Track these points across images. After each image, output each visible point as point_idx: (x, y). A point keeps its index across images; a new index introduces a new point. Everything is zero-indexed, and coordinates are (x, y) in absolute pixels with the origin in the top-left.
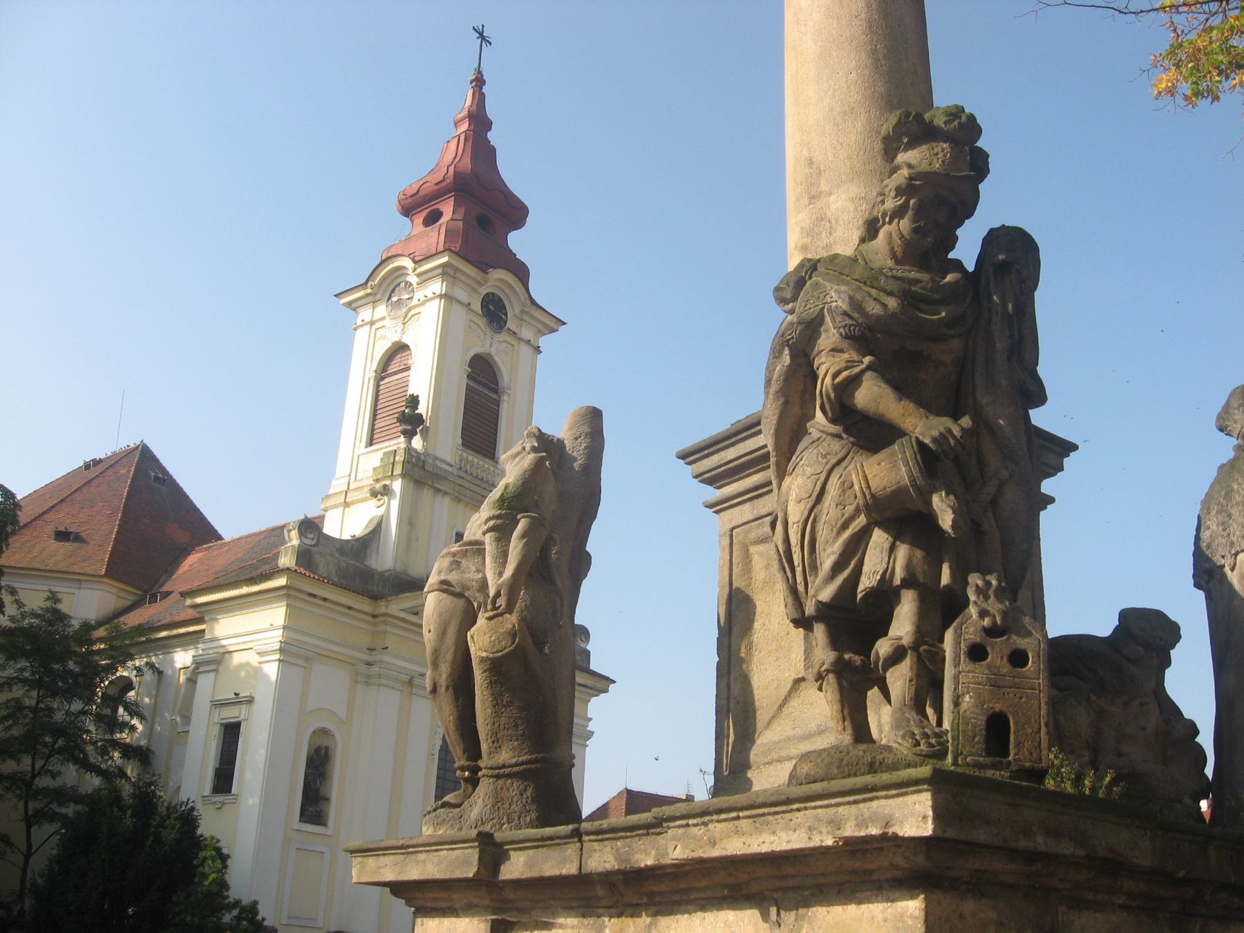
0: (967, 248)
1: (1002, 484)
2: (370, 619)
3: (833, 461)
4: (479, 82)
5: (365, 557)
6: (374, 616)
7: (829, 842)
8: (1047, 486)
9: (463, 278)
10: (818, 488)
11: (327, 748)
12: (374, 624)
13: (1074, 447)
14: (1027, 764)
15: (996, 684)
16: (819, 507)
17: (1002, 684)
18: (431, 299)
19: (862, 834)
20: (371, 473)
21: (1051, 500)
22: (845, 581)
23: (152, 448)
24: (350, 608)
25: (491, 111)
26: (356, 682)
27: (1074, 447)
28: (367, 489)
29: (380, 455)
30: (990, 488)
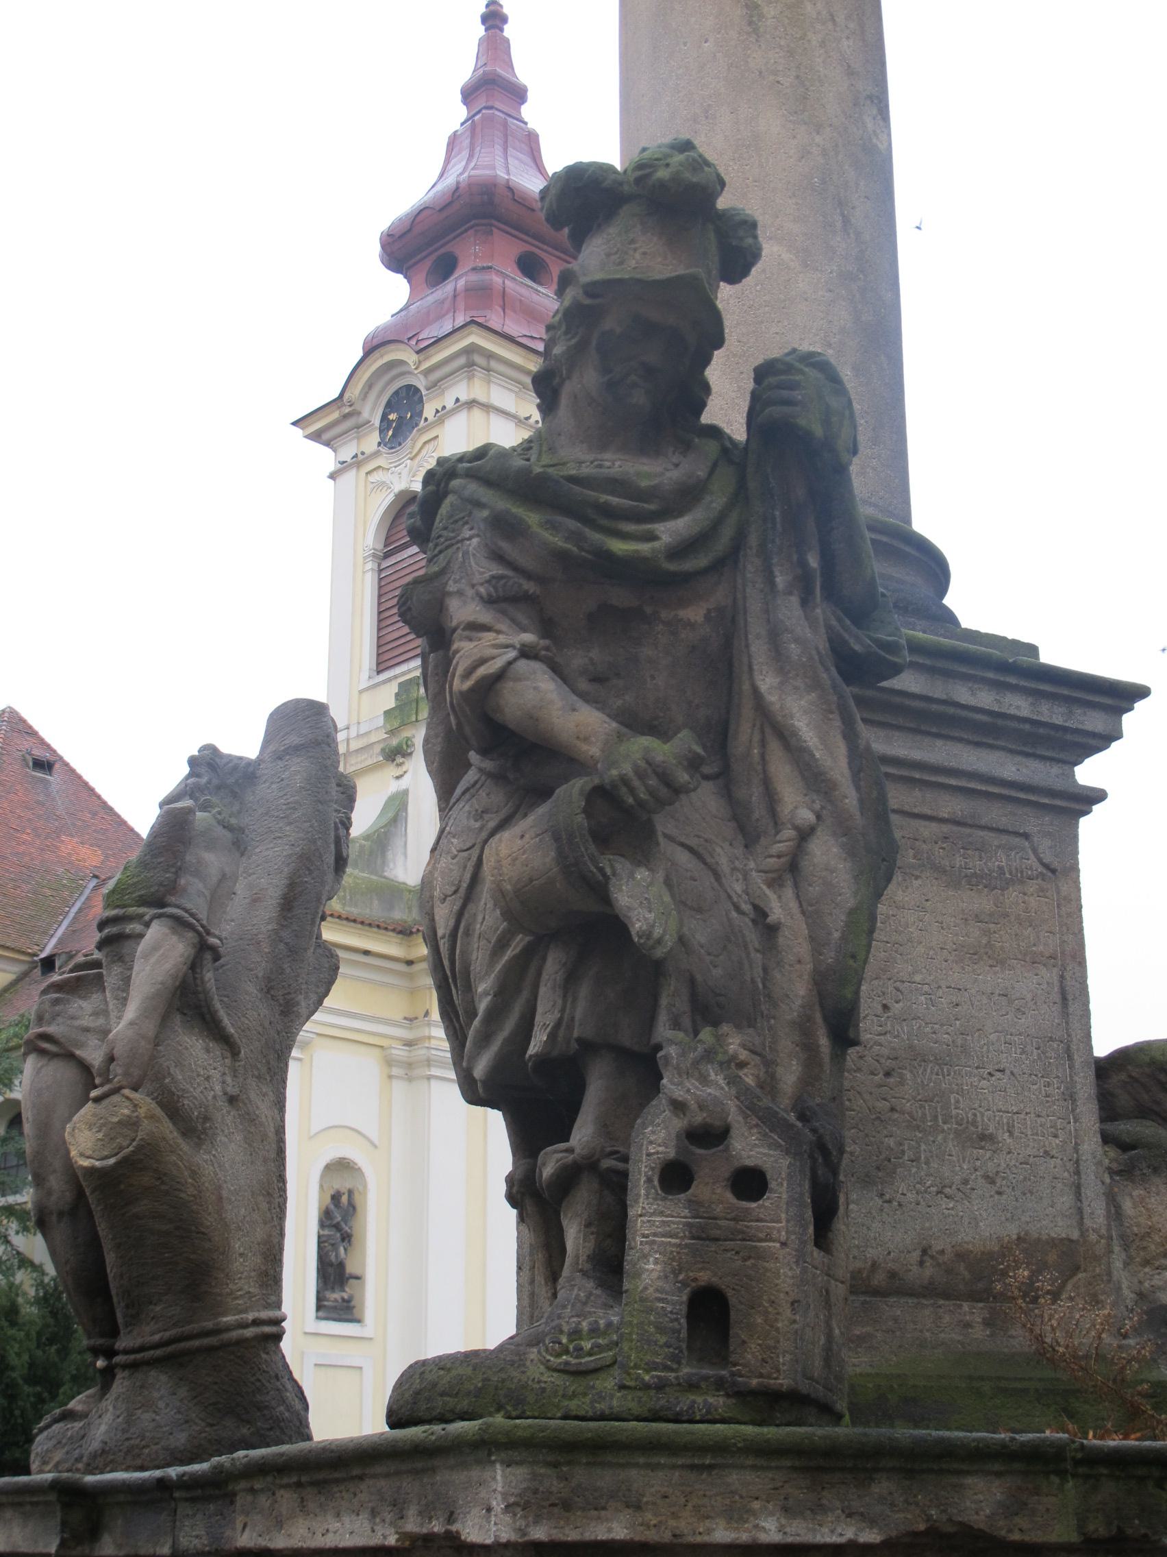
0: (727, 406)
1: (804, 835)
2: (402, 967)
3: (492, 824)
4: (494, 19)
5: (384, 863)
6: (410, 963)
7: (392, 1540)
8: (1088, 773)
9: (501, 368)
10: (468, 876)
11: (350, 1193)
12: (411, 977)
13: (1141, 692)
14: (754, 1382)
15: (703, 1234)
16: (471, 907)
17: (716, 1233)
18: (454, 411)
19: (425, 1531)
20: (381, 721)
21: (1098, 796)
22: (507, 1041)
23: (25, 714)
24: (367, 953)
25: (525, 66)
26: (390, 1077)
27: (1141, 692)
28: (377, 749)
29: (394, 688)
30: (784, 841)
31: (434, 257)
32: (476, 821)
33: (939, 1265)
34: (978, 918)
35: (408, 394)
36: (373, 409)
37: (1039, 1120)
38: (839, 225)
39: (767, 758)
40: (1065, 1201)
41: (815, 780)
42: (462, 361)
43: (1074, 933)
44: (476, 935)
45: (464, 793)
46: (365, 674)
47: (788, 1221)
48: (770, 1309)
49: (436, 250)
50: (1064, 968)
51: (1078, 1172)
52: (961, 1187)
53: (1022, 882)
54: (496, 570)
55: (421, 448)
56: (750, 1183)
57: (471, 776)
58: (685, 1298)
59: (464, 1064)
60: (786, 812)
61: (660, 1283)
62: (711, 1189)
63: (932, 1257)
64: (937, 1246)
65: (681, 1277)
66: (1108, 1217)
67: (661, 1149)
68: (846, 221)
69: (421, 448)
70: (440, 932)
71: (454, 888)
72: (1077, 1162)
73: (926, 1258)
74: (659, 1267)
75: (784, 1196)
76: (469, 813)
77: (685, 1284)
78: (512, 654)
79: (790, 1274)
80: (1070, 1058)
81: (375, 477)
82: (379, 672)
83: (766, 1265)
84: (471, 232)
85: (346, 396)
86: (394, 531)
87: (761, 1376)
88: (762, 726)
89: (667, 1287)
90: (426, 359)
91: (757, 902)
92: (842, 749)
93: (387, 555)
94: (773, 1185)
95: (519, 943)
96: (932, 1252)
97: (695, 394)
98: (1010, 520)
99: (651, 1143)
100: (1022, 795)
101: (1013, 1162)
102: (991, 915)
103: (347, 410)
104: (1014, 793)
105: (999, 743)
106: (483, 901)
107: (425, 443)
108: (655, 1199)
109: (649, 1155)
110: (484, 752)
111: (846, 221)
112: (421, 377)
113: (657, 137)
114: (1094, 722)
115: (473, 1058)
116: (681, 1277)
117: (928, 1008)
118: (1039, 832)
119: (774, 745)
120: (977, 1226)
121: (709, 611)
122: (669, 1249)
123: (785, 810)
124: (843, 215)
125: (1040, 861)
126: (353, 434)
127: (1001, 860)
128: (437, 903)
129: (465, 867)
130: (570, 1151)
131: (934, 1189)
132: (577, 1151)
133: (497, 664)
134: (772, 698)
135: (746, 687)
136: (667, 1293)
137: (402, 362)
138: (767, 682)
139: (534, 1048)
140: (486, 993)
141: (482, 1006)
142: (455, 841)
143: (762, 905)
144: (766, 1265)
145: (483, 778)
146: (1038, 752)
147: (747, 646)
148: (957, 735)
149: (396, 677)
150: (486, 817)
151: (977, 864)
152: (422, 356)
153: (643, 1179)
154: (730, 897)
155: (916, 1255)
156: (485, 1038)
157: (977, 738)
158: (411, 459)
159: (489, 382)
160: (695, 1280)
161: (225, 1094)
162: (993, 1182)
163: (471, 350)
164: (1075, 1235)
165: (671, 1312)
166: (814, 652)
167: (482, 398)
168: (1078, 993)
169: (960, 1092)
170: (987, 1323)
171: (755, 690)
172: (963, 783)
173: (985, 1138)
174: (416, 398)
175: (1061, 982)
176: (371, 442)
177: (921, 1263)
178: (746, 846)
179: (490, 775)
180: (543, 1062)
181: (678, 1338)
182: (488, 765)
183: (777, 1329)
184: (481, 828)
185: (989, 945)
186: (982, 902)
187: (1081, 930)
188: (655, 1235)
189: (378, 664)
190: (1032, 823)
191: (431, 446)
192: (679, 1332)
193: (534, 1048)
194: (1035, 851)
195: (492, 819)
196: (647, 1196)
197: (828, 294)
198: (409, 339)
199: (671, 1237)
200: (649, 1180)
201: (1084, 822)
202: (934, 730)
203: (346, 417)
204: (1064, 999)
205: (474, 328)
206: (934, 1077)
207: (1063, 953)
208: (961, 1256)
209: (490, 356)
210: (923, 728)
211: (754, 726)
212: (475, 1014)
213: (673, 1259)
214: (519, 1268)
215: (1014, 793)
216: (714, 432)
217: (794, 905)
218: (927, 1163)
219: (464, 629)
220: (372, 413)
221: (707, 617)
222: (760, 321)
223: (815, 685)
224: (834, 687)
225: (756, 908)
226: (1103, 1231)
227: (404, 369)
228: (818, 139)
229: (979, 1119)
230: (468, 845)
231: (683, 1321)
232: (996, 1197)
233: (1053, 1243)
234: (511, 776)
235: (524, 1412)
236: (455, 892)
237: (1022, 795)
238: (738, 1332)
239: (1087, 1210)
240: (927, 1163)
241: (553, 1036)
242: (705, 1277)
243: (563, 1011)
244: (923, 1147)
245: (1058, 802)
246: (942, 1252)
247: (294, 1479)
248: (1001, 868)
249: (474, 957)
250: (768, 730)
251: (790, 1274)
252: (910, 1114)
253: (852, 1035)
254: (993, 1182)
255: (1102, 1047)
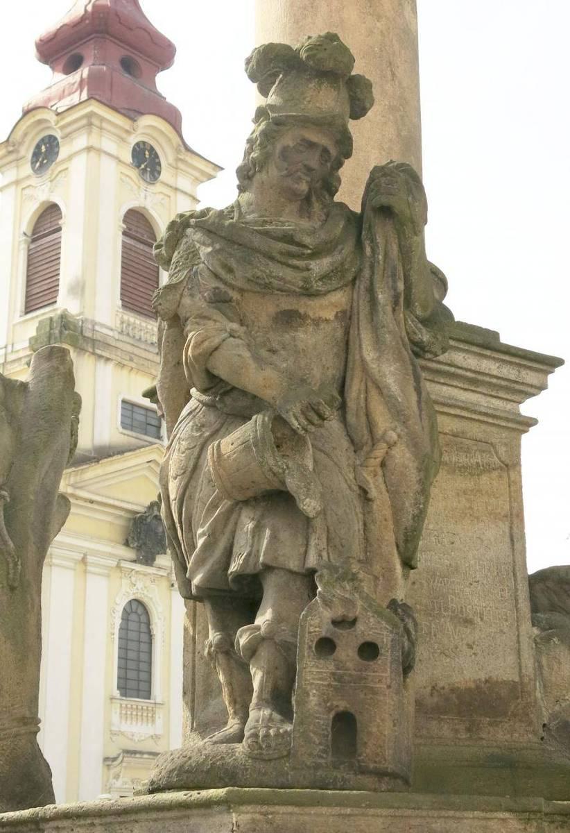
0: (351, 194)
1: (391, 446)
3: (207, 434)
8: (527, 408)
10: (191, 464)
15: (340, 682)
16: (193, 483)
21: (529, 423)
24: (92, 502)
29: (35, 324)
31: (69, 55)
32: (197, 431)
33: (441, 695)
34: (465, 493)
35: (49, 140)
36: (27, 150)
37: (497, 611)
38: (389, 77)
39: (369, 400)
40: (511, 659)
41: (398, 413)
42: (84, 122)
43: (518, 502)
44: (196, 499)
45: (189, 414)
46: (18, 314)
47: (391, 672)
48: (381, 724)
49: (69, 52)
50: (512, 523)
51: (518, 642)
52: (454, 650)
53: (489, 471)
54: (215, 284)
55: (57, 175)
56: (369, 650)
57: (192, 404)
58: (331, 716)
59: (187, 575)
60: (380, 433)
61: (316, 708)
62: (347, 652)
63: (437, 691)
64: (441, 684)
65: (328, 704)
66: (535, 669)
67: (317, 629)
68: (393, 75)
69: (57, 175)
70: (172, 497)
71: (182, 471)
72: (518, 636)
73: (434, 691)
74: (316, 699)
75: (389, 658)
76: (193, 426)
77: (330, 709)
78: (225, 335)
79: (392, 703)
80: (515, 575)
81: (26, 192)
82: (27, 313)
83: (378, 697)
84: (92, 42)
85: (10, 139)
86: (38, 226)
87: (375, 762)
88: (366, 380)
89: (320, 710)
90: (63, 119)
91: (361, 484)
92: (414, 398)
93: (34, 241)
94: (382, 651)
95: (226, 504)
96: (437, 688)
97: (330, 185)
98: (489, 259)
99: (311, 625)
100: (490, 420)
101: (483, 636)
102: (472, 491)
103: (11, 149)
104: (485, 419)
105: (479, 389)
106: (201, 479)
107: (60, 172)
108: (313, 659)
109: (310, 633)
110: (204, 391)
111: (393, 75)
112: (59, 131)
113: (318, 30)
114: (530, 377)
115: (194, 573)
116: (328, 704)
117: (436, 545)
118: (499, 442)
119: (373, 393)
120: (463, 673)
121: (337, 313)
122: (322, 688)
123: (379, 432)
124: (392, 71)
125: (499, 459)
126: (14, 164)
127: (478, 458)
128: (171, 479)
129: (190, 459)
130: (258, 628)
131: (439, 651)
132: (263, 629)
133: (217, 341)
134: (373, 366)
135: (357, 357)
136: (320, 714)
137: (46, 121)
138: (369, 354)
139: (233, 568)
140: (203, 534)
141: (200, 542)
142: (184, 443)
143: (365, 487)
144: (378, 697)
145: (201, 405)
146: (500, 395)
147: (359, 334)
148: (455, 384)
149: (37, 317)
150: (204, 430)
151: (463, 460)
152: (60, 117)
153: (306, 646)
154: (346, 481)
155: (429, 689)
156: (201, 562)
157: (466, 386)
158: (51, 181)
159: (101, 136)
160: (337, 706)
161: (8, 585)
162: (472, 648)
163: (90, 115)
164: (517, 679)
165: (323, 725)
166: (399, 339)
167: (96, 145)
168: (519, 537)
169: (454, 594)
170: (469, 730)
171: (363, 360)
172: (458, 412)
173: (468, 622)
174: (55, 144)
175: (510, 531)
176: (27, 169)
177: (432, 695)
178: (355, 452)
179: (204, 404)
180: (239, 577)
181: (327, 740)
182: (205, 398)
183: (385, 736)
184: (201, 436)
185: (471, 508)
186: (468, 484)
187: (522, 500)
188: (314, 679)
189: (26, 308)
190: (497, 436)
191: (63, 174)
192: (327, 736)
193: (233, 568)
194: (497, 453)
195: (207, 431)
196: (309, 657)
197: (382, 119)
198: (52, 106)
199: (323, 681)
200: (310, 647)
201: (524, 437)
202: (442, 381)
203: (10, 152)
204: (512, 540)
205: (93, 102)
206: (439, 585)
207: (511, 514)
208: (453, 690)
209: (102, 119)
210: (436, 380)
211: (361, 381)
212: (194, 548)
213: (324, 694)
214: (185, 693)
215: (485, 419)
216: (342, 206)
217: (383, 487)
218: (435, 635)
219: (195, 318)
220: (27, 151)
221: (336, 316)
222: (370, 144)
223: (400, 358)
224: (411, 359)
225: (360, 487)
226: (532, 676)
227: (49, 125)
228: (378, 24)
229: (464, 610)
230: (192, 445)
231: (329, 730)
232: (473, 656)
233: (504, 682)
234: (219, 406)
235: (236, 783)
236: (183, 473)
237: (490, 420)
238: (362, 736)
239: (523, 665)
240: (435, 635)
241: (246, 560)
242: (342, 705)
243: (252, 546)
244: (433, 626)
245: (510, 425)
246: (443, 688)
247: (89, 821)
248: (477, 463)
249: (194, 512)
250: (370, 384)
251: (392, 703)
252: (426, 606)
253: (413, 563)
254: (472, 648)
255: (532, 569)
